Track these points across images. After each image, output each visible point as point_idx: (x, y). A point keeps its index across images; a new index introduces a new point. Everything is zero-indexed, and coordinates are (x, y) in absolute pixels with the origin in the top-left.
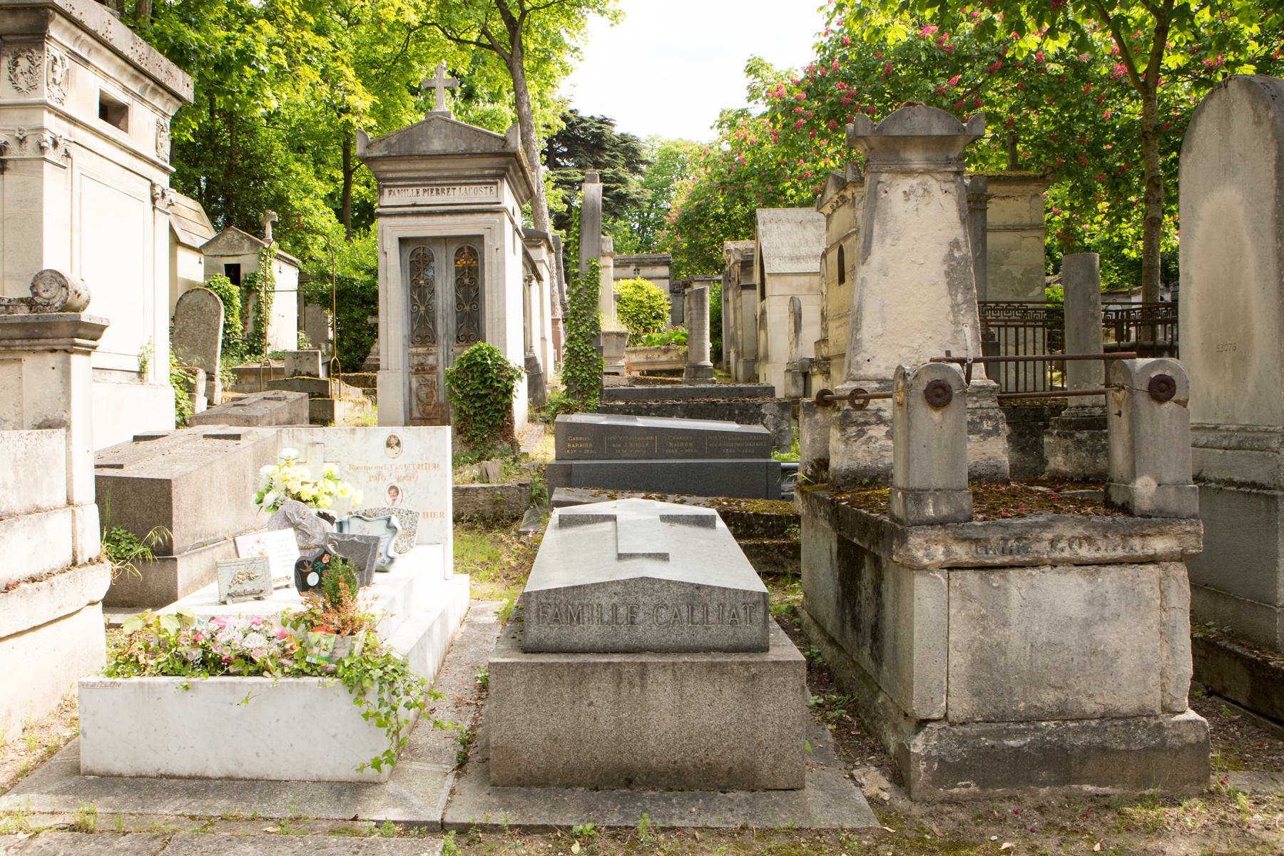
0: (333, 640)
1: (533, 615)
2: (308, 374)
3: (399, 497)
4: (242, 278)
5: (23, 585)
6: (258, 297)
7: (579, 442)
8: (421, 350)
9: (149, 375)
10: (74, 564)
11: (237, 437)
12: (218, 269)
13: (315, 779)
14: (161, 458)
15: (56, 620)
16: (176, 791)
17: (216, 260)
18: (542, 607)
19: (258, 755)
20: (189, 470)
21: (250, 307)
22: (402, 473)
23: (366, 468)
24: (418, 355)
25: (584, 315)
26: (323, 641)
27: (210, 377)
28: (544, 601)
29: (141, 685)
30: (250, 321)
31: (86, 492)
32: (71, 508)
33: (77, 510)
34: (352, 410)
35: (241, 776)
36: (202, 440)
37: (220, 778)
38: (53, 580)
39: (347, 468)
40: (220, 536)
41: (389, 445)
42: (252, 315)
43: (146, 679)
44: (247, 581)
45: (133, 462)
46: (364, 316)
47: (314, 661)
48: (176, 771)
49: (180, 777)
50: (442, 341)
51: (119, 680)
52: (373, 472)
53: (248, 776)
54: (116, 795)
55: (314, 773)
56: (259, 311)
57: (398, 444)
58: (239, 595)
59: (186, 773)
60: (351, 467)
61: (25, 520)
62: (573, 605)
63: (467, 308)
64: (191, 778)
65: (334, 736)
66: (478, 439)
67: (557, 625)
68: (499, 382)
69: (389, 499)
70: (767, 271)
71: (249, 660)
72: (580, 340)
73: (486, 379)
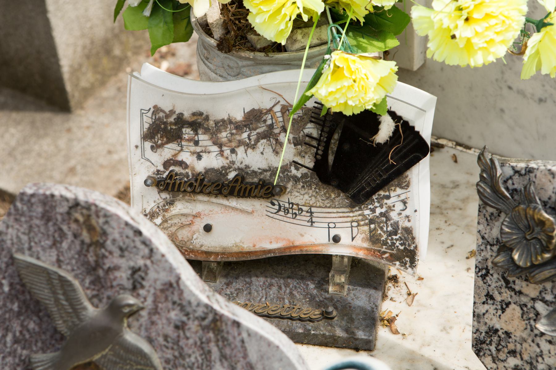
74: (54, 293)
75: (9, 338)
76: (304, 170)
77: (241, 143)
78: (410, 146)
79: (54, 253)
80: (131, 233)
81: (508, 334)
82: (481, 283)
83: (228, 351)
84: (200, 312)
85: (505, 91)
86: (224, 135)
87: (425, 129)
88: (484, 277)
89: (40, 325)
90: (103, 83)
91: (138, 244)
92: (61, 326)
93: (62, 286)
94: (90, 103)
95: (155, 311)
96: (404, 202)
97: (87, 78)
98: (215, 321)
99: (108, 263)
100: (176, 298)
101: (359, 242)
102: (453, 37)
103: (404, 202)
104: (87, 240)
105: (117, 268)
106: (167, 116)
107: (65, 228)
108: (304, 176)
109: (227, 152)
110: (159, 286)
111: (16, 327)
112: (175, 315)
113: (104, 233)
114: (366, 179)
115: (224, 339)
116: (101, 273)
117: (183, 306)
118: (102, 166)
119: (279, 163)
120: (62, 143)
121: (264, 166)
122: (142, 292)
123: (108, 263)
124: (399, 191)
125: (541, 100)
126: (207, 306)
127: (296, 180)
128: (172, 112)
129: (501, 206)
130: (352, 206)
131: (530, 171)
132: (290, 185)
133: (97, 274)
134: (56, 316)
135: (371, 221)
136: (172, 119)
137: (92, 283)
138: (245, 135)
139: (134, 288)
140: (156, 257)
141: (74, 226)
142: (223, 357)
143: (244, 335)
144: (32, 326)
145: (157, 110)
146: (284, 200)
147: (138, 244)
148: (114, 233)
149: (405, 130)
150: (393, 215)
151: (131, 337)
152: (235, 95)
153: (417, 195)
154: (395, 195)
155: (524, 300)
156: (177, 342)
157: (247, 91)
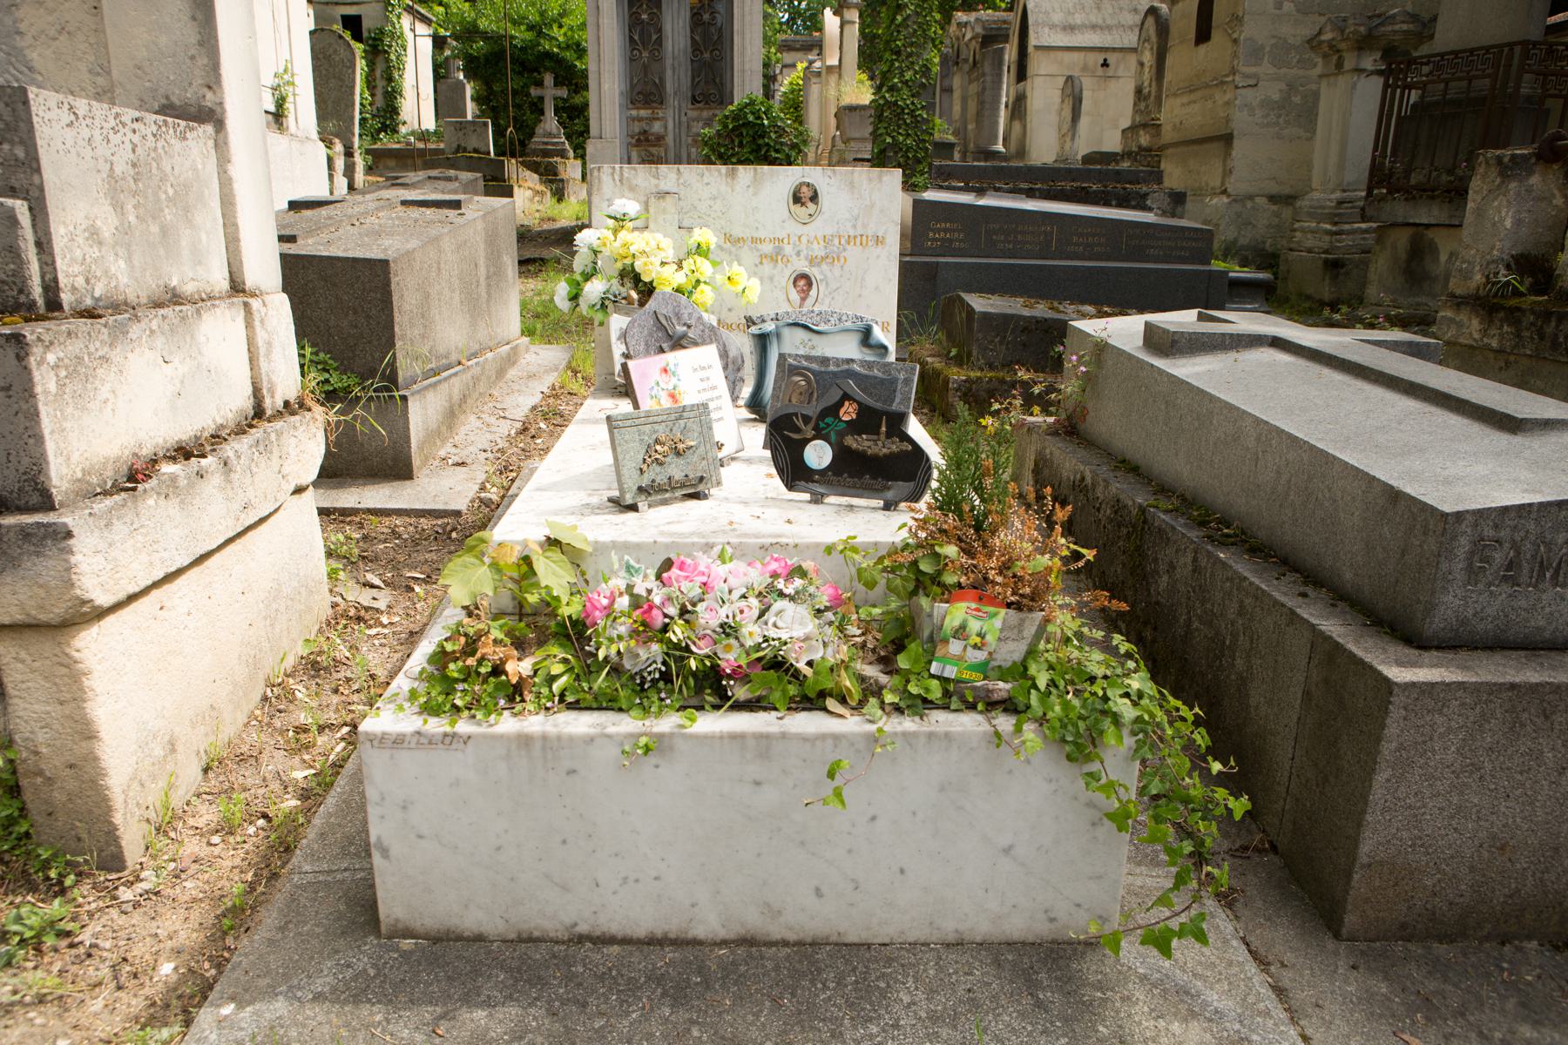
0: (997, 623)
1: (1459, 566)
2: (476, 151)
3: (813, 292)
4: (365, 34)
5: (167, 468)
6: (388, 60)
7: (946, 230)
8: (643, 113)
9: (290, 121)
10: (259, 413)
11: (456, 205)
12: (334, 21)
13: (951, 938)
14: (354, 230)
15: (240, 535)
16: (632, 989)
17: (329, 9)
18: (1480, 548)
19: (818, 892)
20: (410, 246)
21: (378, 73)
22: (818, 250)
23: (754, 240)
24: (640, 119)
25: (910, 55)
26: (974, 626)
27: (349, 154)
28: (1489, 532)
29: (525, 740)
30: (379, 92)
31: (263, 269)
32: (239, 300)
33: (255, 304)
34: (531, 200)
35: (777, 936)
36: (400, 208)
37: (724, 943)
38: (228, 450)
40: (454, 358)
41: (797, 199)
42: (380, 83)
43: (535, 723)
44: (671, 458)
45: (309, 233)
46: (526, 86)
47: (951, 672)
48: (615, 928)
49: (625, 941)
50: (672, 101)
51: (463, 727)
52: (768, 248)
53: (792, 937)
54: (489, 1004)
55: (949, 927)
56: (390, 79)
57: (814, 198)
58: (661, 490)
59: (641, 932)
61: (154, 319)
62: (1548, 545)
63: (707, 55)
64: (654, 942)
65: (1007, 850)
67: (1507, 588)
68: (777, 151)
69: (795, 296)
70: (1033, 41)
71: (778, 665)
72: (905, 91)
73: (759, 147)
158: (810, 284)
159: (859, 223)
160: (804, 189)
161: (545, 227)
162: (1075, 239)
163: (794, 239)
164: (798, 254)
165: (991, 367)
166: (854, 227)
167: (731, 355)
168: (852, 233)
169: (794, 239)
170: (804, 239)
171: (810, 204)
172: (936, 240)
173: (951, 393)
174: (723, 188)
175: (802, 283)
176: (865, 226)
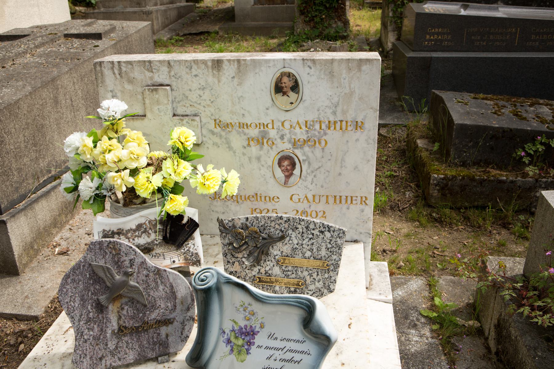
3: (297, 171)
7: (438, 34)
11: (98, 36)
22: (301, 134)
23: (242, 125)
36: (63, 40)
39: (212, 126)
41: (279, 89)
52: (254, 132)
57: (295, 87)
60: (218, 123)
66: (317, 20)
74: (105, 273)
75: (90, 294)
76: (159, 241)
77: (136, 236)
78: (193, 225)
79: (104, 260)
80: (128, 248)
81: (236, 272)
82: (225, 258)
83: (163, 280)
84: (153, 270)
85: (212, 212)
86: (129, 235)
87: (196, 219)
88: (225, 256)
89: (100, 287)
90: (31, 261)
91: (131, 251)
92: (108, 284)
93: (108, 270)
94: (27, 270)
95: (139, 272)
96: (194, 245)
97: (25, 260)
98: (158, 271)
99: (122, 260)
100: (145, 266)
101: (181, 261)
102: (204, 185)
103: (194, 245)
104: (114, 253)
105: (125, 261)
106: (108, 232)
107: (107, 251)
108: (160, 243)
109: (131, 240)
110: (139, 264)
111: (92, 289)
112: (145, 272)
113: (120, 250)
114: (181, 239)
115: (162, 277)
116: (120, 263)
117: (147, 269)
118: (40, 293)
119: (149, 240)
120: (18, 288)
121: (145, 242)
122: (134, 267)
123: (122, 260)
124: (191, 241)
125: (223, 213)
126: (155, 267)
127: (157, 245)
128: (110, 230)
129: (227, 232)
130: (177, 250)
131: (233, 220)
132: (155, 247)
133: (118, 264)
134: (107, 281)
135: (184, 253)
136: (110, 233)
137: (117, 267)
138: (137, 233)
139: (131, 266)
140: (137, 254)
141: (110, 250)
142: (162, 282)
143: (168, 274)
144: (97, 287)
145: (104, 230)
146: (154, 253)
147: (131, 251)
148: (123, 249)
149: (191, 220)
150: (191, 250)
151: (132, 283)
152: (131, 221)
153: (197, 244)
154: (190, 243)
155: (239, 259)
156: (147, 281)
157: (136, 218)
158: (293, 165)
159: (339, 110)
160: (285, 79)
161: (220, 7)
162: (533, 37)
163: (277, 124)
164: (282, 137)
165: (464, 164)
166: (334, 113)
167: (179, 295)
168: (332, 119)
169: (277, 124)
170: (287, 125)
171: (291, 94)
172: (432, 40)
173: (431, 187)
174: (210, 79)
175: (286, 163)
176: (344, 112)
